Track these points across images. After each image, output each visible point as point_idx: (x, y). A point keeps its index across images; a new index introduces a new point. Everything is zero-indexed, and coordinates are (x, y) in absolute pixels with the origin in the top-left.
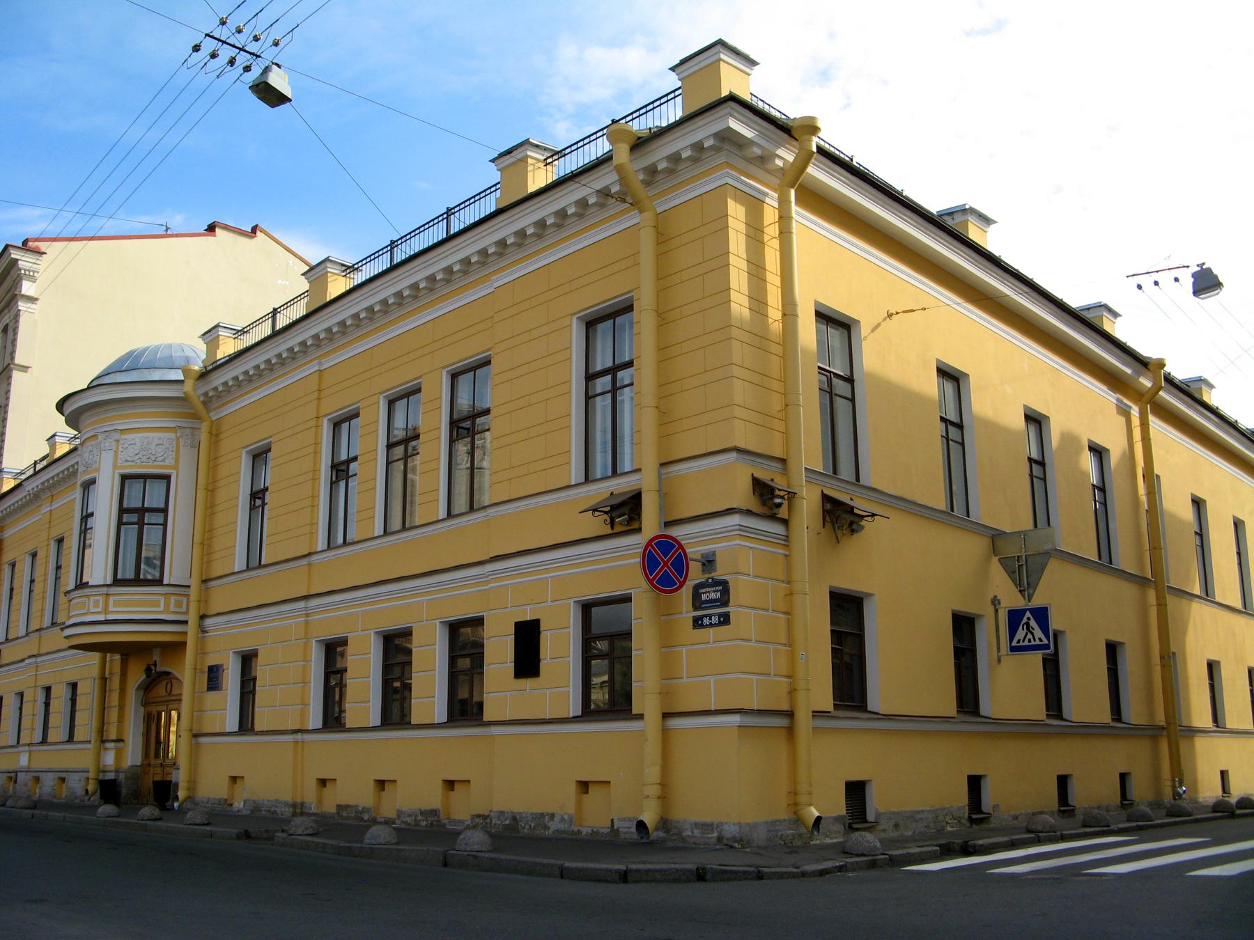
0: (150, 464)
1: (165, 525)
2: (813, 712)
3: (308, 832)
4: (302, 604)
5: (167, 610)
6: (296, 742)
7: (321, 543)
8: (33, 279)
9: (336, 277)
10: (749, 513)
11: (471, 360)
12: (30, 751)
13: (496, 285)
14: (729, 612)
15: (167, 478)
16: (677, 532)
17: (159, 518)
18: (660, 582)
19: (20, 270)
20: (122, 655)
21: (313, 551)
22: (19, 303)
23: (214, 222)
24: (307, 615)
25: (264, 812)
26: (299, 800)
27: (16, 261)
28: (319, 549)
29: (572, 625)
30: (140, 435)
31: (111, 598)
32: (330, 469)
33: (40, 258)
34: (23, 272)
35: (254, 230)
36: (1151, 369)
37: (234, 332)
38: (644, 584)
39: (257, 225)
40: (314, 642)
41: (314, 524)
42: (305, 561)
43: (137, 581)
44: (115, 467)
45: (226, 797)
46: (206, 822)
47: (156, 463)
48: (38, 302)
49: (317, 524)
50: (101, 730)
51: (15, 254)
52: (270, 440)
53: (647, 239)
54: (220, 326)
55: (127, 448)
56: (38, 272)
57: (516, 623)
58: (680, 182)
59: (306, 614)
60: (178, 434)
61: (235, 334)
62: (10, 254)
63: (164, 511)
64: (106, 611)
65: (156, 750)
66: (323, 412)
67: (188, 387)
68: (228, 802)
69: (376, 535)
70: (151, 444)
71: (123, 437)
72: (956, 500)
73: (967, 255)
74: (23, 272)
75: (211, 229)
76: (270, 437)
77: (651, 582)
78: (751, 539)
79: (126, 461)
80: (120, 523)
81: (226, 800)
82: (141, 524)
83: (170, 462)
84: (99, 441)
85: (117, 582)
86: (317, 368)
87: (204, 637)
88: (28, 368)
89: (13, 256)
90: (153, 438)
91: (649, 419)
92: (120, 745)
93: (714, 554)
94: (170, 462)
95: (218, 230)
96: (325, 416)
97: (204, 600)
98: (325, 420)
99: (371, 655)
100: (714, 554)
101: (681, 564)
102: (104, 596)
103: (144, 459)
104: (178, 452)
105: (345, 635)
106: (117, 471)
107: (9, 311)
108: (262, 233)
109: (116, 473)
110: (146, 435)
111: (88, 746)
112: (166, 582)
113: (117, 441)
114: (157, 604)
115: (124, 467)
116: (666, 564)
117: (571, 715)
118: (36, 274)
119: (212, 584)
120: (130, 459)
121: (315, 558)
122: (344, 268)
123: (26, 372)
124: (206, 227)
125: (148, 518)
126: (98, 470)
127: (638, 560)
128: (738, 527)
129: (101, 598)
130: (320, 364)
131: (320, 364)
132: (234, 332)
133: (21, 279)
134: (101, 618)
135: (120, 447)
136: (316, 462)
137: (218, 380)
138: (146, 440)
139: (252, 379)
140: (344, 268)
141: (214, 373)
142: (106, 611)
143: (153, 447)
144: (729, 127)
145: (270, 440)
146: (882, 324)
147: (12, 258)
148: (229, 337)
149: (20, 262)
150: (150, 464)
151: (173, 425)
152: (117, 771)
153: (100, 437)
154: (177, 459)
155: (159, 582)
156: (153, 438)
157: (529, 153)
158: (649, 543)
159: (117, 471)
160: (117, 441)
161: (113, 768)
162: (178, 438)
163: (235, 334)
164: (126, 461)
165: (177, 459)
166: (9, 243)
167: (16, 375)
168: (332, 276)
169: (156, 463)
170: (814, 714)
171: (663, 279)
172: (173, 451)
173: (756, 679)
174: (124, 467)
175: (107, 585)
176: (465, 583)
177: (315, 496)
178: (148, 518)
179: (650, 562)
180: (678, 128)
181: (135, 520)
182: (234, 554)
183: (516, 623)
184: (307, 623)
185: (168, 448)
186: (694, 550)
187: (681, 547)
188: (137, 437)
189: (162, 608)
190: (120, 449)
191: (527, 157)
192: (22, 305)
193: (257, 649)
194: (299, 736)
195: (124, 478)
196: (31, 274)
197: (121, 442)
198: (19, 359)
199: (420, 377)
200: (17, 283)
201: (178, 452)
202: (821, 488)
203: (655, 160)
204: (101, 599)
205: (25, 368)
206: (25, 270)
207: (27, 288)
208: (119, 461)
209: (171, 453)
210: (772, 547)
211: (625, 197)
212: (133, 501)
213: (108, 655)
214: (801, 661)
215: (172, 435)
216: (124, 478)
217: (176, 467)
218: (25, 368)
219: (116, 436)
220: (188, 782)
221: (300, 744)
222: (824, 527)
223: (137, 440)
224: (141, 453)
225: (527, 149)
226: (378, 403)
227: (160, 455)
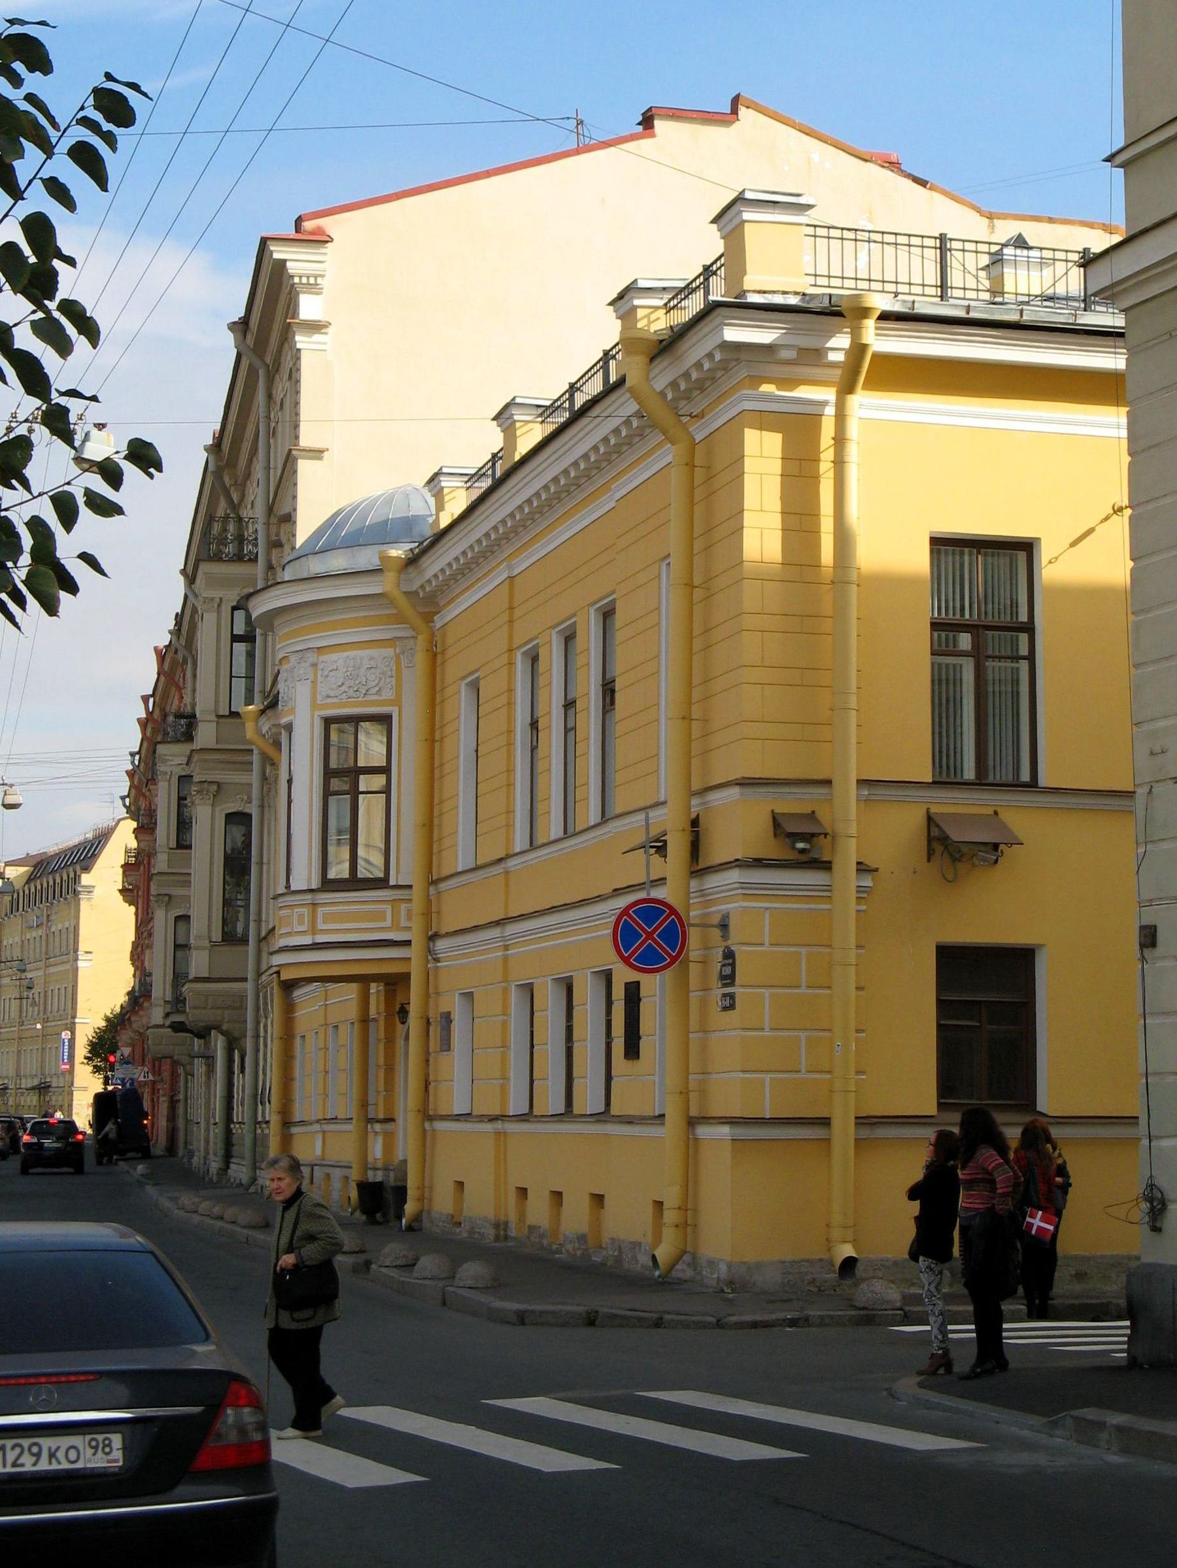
0: (359, 699)
1: (387, 791)
2: (856, 1118)
3: (398, 1263)
4: (496, 932)
5: (395, 926)
6: (498, 1134)
7: (520, 841)
8: (314, 288)
9: (531, 425)
10: (758, 863)
11: (605, 602)
12: (324, 1132)
13: (618, 496)
14: (734, 993)
15: (384, 720)
17: (379, 781)
18: (642, 959)
19: (292, 277)
20: (386, 984)
21: (511, 852)
22: (297, 338)
23: (650, 109)
24: (506, 947)
25: (476, 1236)
26: (503, 1218)
27: (284, 261)
28: (517, 850)
29: (658, 994)
31: (320, 909)
32: (529, 728)
33: (322, 250)
34: (296, 280)
35: (736, 102)
37: (466, 479)
39: (739, 94)
40: (513, 988)
42: (498, 869)
43: (354, 883)
44: (314, 706)
45: (451, 1212)
46: (357, 1249)
47: (369, 698)
48: (330, 330)
49: (514, 811)
50: (364, 1104)
52: (476, 675)
54: (442, 473)
55: (327, 676)
56: (322, 276)
57: (626, 984)
58: (724, 394)
59: (505, 945)
60: (397, 650)
61: (466, 482)
62: (272, 252)
63: (386, 770)
64: (314, 930)
66: (516, 644)
67: (390, 577)
68: (454, 1220)
69: (552, 838)
70: (359, 668)
71: (322, 658)
74: (296, 280)
75: (647, 121)
76: (537, 638)
78: (772, 897)
79: (328, 697)
80: (327, 793)
81: (453, 1217)
82: (355, 793)
83: (388, 694)
84: (291, 664)
85: (328, 885)
86: (505, 575)
87: (437, 967)
88: (322, 452)
89: (276, 256)
90: (361, 659)
91: (667, 735)
92: (389, 1126)
94: (388, 694)
95: (657, 123)
96: (519, 647)
97: (429, 912)
99: (549, 1012)
102: (310, 907)
103: (351, 693)
104: (399, 678)
105: (530, 981)
106: (317, 713)
108: (750, 110)
109: (316, 717)
110: (351, 653)
111: (349, 1127)
112: (392, 882)
113: (314, 665)
114: (381, 916)
115: (325, 707)
116: (649, 935)
117: (657, 1114)
118: (319, 280)
119: (443, 886)
120: (332, 693)
121: (511, 863)
122: (540, 410)
123: (320, 458)
124: (641, 118)
125: (364, 782)
127: (610, 931)
128: (737, 885)
129: (306, 910)
130: (510, 567)
132: (466, 479)
133: (298, 294)
134: (307, 940)
135: (319, 677)
136: (510, 719)
137: (436, 564)
138: (352, 663)
139: (467, 568)
140: (540, 410)
141: (423, 559)
142: (314, 930)
143: (362, 671)
144: (726, 341)
145: (476, 675)
146: (1096, 528)
147: (275, 259)
148: (458, 488)
149: (289, 264)
150: (359, 699)
152: (386, 1169)
153: (293, 659)
154: (399, 688)
155: (381, 883)
156: (361, 659)
157: (636, 302)
160: (314, 665)
161: (380, 1165)
162: (397, 656)
163: (466, 482)
164: (328, 697)
165: (399, 688)
166: (265, 234)
167: (304, 467)
168: (521, 427)
169: (369, 698)
170: (859, 1121)
172: (392, 677)
173: (770, 1078)
174: (325, 707)
175: (311, 891)
176: (542, 935)
178: (364, 782)
180: (703, 324)
181: (346, 787)
182: (456, 845)
183: (626, 984)
184: (506, 959)
185: (383, 673)
188: (337, 658)
189: (388, 923)
190: (320, 679)
191: (635, 308)
192: (301, 341)
193: (571, 977)
194: (499, 1125)
195: (328, 722)
196: (312, 280)
197: (320, 667)
198: (307, 438)
199: (574, 615)
200: (292, 307)
201: (399, 678)
202: (925, 807)
203: (687, 367)
204: (305, 910)
205: (317, 454)
206: (300, 277)
207: (309, 307)
208: (319, 697)
209: (388, 680)
210: (796, 903)
214: (837, 1054)
215: (389, 652)
216: (328, 722)
217: (397, 702)
218: (317, 454)
219: (311, 657)
220: (418, 1188)
221: (502, 1135)
222: (929, 860)
223: (341, 663)
224: (348, 683)
225: (632, 298)
227: (373, 684)
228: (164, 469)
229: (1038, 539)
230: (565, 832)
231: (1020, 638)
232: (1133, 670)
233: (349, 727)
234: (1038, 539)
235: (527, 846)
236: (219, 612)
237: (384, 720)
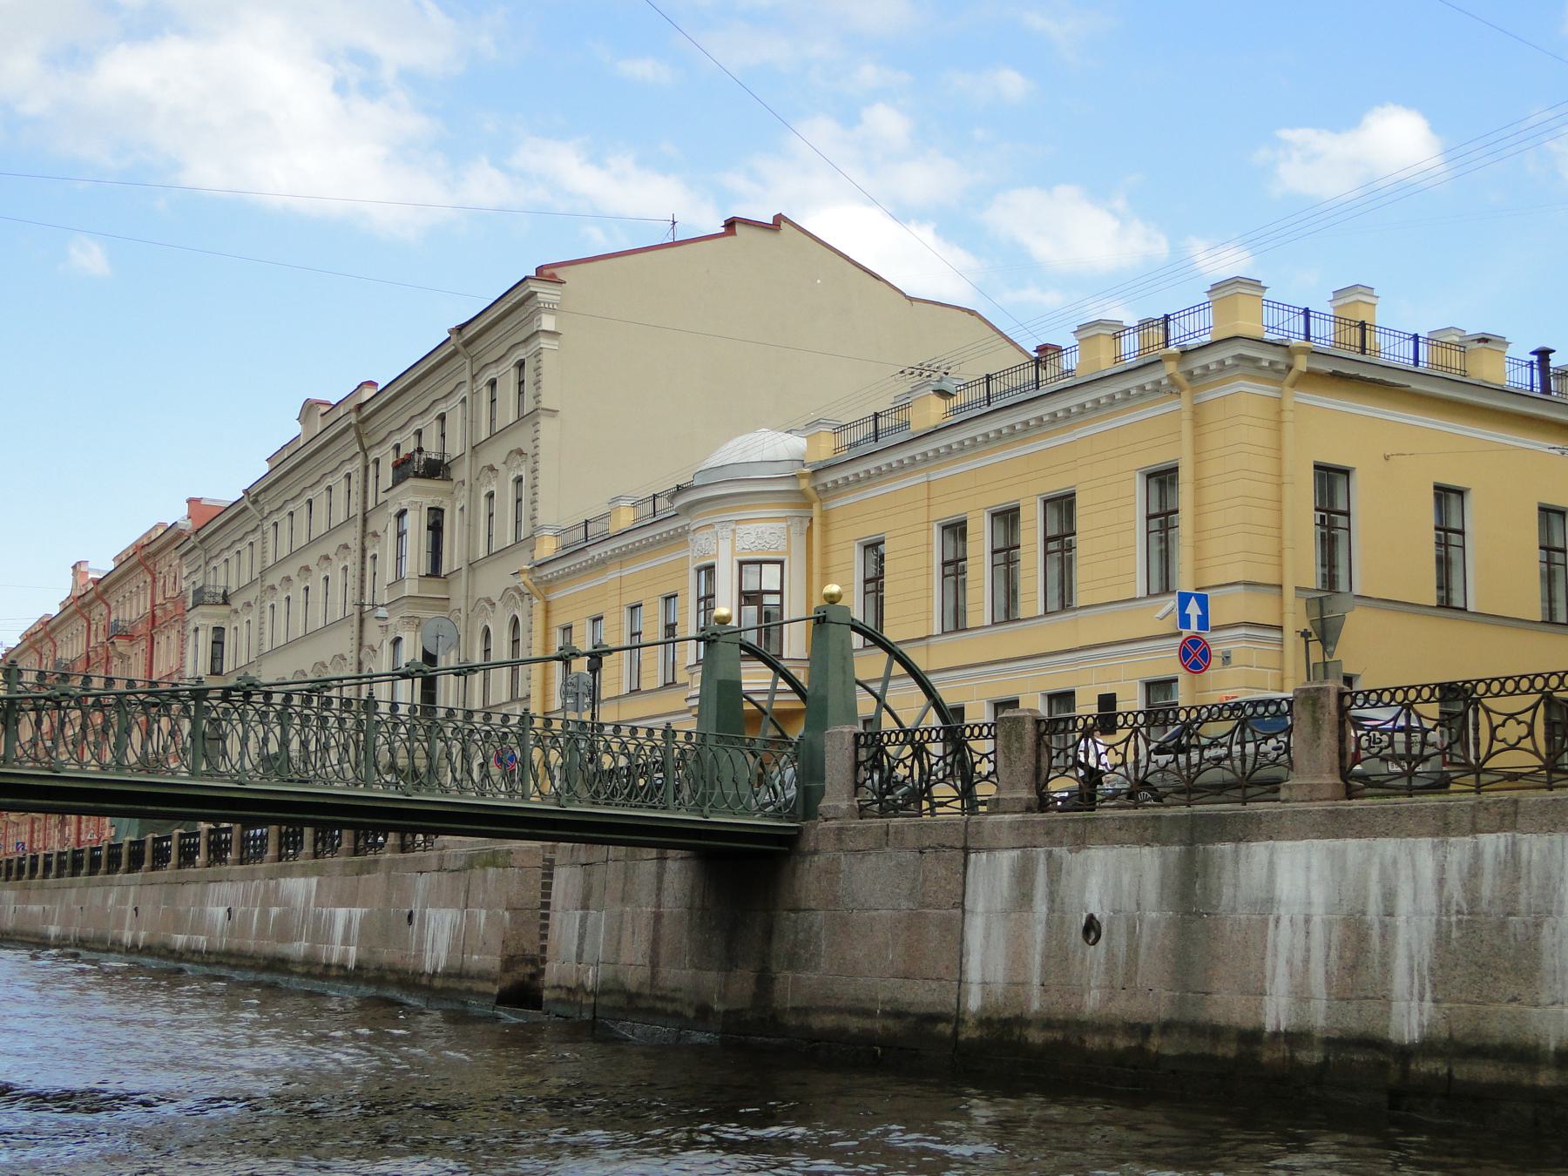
15: (781, 563)
16: (1207, 636)
30: (756, 525)
36: (813, 904)
38: (1183, 669)
41: (929, 611)
51: (533, 286)
53: (1186, 415)
63: (780, 593)
65: (1448, 590)
72: (529, 851)
73: (1224, 803)
77: (1185, 666)
86: (925, 479)
93: (1229, 652)
98: (935, 525)
100: (1229, 652)
101: (1206, 655)
106: (735, 558)
107: (526, 346)
126: (716, 556)
127: (1177, 654)
131: (928, 476)
151: (784, 515)
158: (1184, 642)
159: (735, 558)
160: (734, 530)
162: (788, 527)
171: (1198, 454)
174: (741, 554)
177: (929, 589)
179: (1184, 654)
183: (1099, 696)
186: (1216, 650)
187: (1205, 643)
211: (1174, 388)
212: (751, 584)
213: (84, 817)
215: (784, 525)
216: (741, 563)
217: (788, 552)
226: (983, 516)
228: (1432, 491)
229: (1539, 503)
230: (1148, 593)
231: (417, 590)
232: (528, 448)
233: (756, 568)
234: (1539, 503)
235: (1145, 595)
236: (420, 511)
237: (781, 563)
